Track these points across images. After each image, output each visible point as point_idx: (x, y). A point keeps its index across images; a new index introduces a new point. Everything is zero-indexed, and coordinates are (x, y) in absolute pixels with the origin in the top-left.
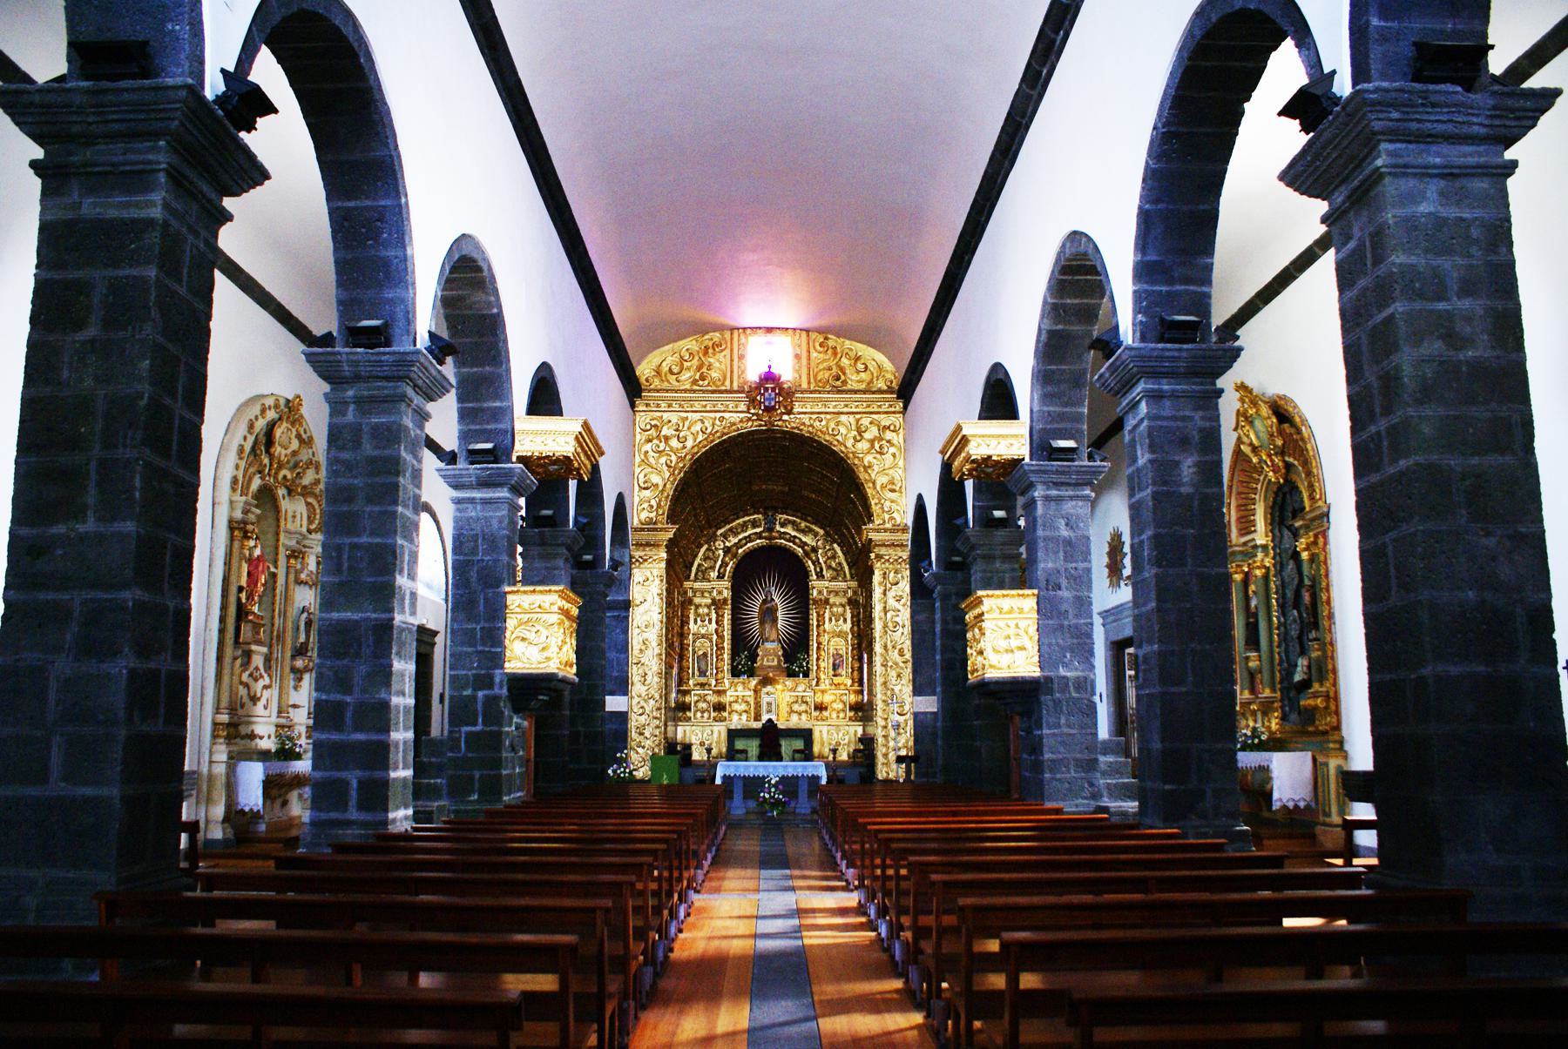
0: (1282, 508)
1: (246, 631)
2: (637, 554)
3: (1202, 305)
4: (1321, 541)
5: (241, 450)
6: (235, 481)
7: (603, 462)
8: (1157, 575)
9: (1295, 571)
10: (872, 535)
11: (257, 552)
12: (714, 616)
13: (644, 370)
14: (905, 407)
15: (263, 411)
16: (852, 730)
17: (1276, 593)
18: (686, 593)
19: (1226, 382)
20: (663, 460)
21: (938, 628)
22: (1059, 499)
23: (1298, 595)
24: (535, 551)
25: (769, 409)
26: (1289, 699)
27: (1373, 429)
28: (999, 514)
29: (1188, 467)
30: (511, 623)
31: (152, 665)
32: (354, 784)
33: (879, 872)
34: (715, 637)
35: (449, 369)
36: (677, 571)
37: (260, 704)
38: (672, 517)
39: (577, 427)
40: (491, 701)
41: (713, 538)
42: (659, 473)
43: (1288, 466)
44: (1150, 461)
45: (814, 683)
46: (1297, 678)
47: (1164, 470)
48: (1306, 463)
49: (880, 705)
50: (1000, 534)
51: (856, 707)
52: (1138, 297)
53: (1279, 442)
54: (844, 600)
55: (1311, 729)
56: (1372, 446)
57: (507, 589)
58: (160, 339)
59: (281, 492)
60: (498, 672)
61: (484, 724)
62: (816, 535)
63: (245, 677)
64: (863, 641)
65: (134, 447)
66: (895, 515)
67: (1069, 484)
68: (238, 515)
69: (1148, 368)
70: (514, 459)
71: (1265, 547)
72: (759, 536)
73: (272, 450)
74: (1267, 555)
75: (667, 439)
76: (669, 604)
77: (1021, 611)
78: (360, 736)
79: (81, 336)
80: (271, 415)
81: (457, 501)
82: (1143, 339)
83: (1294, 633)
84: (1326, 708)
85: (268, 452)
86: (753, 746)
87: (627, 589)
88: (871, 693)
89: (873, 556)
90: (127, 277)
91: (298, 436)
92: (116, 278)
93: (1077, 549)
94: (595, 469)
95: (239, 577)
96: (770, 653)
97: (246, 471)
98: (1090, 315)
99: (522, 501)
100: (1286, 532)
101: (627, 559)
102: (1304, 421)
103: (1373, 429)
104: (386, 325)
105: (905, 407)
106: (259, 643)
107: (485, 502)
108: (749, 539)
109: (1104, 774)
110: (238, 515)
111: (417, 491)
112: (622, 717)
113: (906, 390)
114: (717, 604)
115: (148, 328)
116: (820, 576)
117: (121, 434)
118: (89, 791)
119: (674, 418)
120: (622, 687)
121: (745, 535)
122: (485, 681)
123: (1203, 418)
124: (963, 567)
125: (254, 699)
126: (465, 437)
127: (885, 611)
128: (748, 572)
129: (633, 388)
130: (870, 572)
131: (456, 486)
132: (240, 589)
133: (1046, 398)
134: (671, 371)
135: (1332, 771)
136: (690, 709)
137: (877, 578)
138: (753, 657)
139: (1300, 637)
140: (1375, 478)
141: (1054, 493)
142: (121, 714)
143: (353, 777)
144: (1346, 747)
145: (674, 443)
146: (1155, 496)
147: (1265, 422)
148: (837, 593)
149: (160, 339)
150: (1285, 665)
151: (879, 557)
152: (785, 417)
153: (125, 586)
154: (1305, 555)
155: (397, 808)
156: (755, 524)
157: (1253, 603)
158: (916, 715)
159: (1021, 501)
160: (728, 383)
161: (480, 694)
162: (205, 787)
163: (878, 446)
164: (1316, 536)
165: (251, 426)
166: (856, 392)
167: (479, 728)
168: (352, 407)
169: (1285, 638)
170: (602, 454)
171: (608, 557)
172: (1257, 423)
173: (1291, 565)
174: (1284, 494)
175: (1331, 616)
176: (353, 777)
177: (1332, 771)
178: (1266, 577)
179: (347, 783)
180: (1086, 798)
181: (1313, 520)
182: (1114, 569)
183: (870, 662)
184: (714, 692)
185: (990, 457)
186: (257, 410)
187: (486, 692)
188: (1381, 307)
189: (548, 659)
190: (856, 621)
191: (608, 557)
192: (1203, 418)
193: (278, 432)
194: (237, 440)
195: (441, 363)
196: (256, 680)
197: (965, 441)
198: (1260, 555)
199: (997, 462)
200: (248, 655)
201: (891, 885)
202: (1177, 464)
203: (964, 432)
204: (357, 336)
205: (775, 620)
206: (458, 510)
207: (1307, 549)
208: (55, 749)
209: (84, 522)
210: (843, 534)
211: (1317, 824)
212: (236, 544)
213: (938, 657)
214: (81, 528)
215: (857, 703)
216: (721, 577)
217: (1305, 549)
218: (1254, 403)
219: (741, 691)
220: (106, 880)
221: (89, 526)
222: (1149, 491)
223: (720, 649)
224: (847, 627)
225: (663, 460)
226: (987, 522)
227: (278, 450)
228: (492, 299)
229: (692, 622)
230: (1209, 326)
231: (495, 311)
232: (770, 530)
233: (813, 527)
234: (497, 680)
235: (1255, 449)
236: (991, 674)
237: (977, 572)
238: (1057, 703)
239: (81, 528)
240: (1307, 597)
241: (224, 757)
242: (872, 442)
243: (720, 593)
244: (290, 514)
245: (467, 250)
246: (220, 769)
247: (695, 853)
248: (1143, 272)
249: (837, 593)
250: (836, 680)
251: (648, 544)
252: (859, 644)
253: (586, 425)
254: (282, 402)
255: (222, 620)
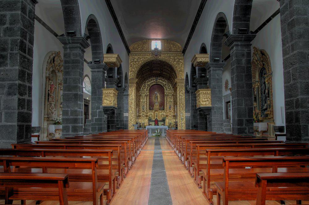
0: (262, 73)
1: (50, 99)
2: (130, 85)
3: (248, 26)
4: (270, 79)
5: (48, 62)
6: (47, 68)
7: (122, 64)
8: (237, 83)
9: (264, 86)
10: (177, 81)
11: (52, 83)
12: (145, 98)
13: (131, 48)
14: (184, 55)
15: (52, 54)
16: (173, 120)
17: (260, 91)
18: (140, 93)
19: (252, 47)
20: (135, 66)
21: (190, 99)
22: (216, 70)
23: (265, 91)
24: (109, 83)
25: (156, 55)
26: (263, 112)
27: (288, 45)
28: (203, 75)
29: (244, 60)
30: (103, 96)
31: (23, 97)
32: (71, 127)
33: (178, 144)
34: (146, 102)
35: (89, 41)
36: (138, 89)
37: (54, 114)
38: (137, 78)
39: (116, 56)
40: (100, 112)
41: (145, 82)
42: (134, 69)
43: (263, 64)
44: (236, 59)
45: (165, 111)
46: (264, 108)
47: (239, 62)
48: (268, 63)
49: (179, 115)
50: (203, 79)
51: (174, 116)
52: (234, 24)
53: (262, 59)
54: (171, 95)
55: (267, 118)
56: (287, 49)
57: (103, 89)
58: (22, 27)
59: (57, 71)
60: (101, 106)
61: (99, 117)
62: (166, 82)
63: (50, 108)
64: (175, 103)
65: (17, 50)
66: (182, 77)
67: (218, 67)
68: (48, 75)
69: (236, 39)
70: (104, 63)
71: (258, 81)
72: (154, 82)
73: (54, 63)
74: (258, 83)
75: (136, 61)
76: (137, 95)
77: (208, 93)
78: (72, 117)
79: (5, 26)
80: (54, 55)
81: (92, 71)
82: (235, 33)
83: (264, 99)
84: (271, 113)
85: (53, 63)
86: (153, 123)
87: (128, 92)
88: (177, 113)
89: (177, 85)
90: (14, 13)
91: (60, 60)
92: (12, 14)
93: (219, 80)
94: (120, 65)
95: (48, 88)
96: (157, 106)
97: (49, 66)
98: (223, 31)
99: (106, 72)
100: (263, 78)
101: (128, 86)
102: (267, 55)
103: (288, 45)
104: (75, 32)
105: (184, 55)
106: (53, 102)
107: (98, 71)
108: (152, 83)
109: (225, 127)
110: (48, 75)
111: (83, 67)
112: (127, 117)
113: (184, 52)
114: (146, 96)
115: (19, 25)
116: (167, 90)
117: (15, 47)
118: (10, 124)
119: (137, 57)
120: (127, 111)
121: (151, 82)
122: (98, 108)
123: (247, 50)
124: (195, 87)
125: (52, 113)
126: (93, 58)
127: (180, 96)
128: (152, 90)
129: (129, 51)
130: (177, 88)
131: (92, 69)
132: (49, 90)
133: (213, 49)
134: (136, 48)
135: (272, 126)
136: (141, 116)
137: (178, 89)
138: (153, 106)
139: (265, 100)
140: (287, 56)
141: (215, 69)
142: (17, 107)
143: (70, 125)
144: (275, 122)
145: (137, 63)
146: (237, 67)
147: (259, 55)
148: (170, 93)
149: (22, 27)
150: (262, 105)
151: (178, 85)
152: (159, 57)
153: (16, 80)
154: (267, 83)
155: (80, 132)
156: (153, 80)
157: (255, 93)
158: (186, 117)
159: (208, 71)
160: (148, 50)
161: (98, 110)
162: (42, 130)
163: (178, 63)
164: (269, 78)
165: (50, 57)
166: (173, 52)
167: (97, 117)
168: (68, 49)
169: (262, 100)
170: (122, 62)
171: (124, 85)
172: (258, 55)
173: (264, 85)
174: (262, 70)
175: (272, 95)
176: (70, 125)
177: (272, 126)
178: (258, 88)
179: (72, 131)
180: (221, 131)
181: (269, 75)
182: (226, 87)
183: (177, 107)
184: (146, 113)
185: (201, 61)
186: (51, 54)
187: (99, 110)
188: (291, 17)
189: (111, 103)
190: (174, 99)
191: (124, 85)
192: (247, 50)
193: (55, 59)
194: (47, 60)
195: (87, 40)
196: (53, 109)
197: (196, 58)
198: (257, 83)
199: (203, 63)
200: (51, 104)
201: (181, 146)
202: (241, 60)
203: (196, 56)
204: (69, 34)
205: (158, 99)
206: (92, 73)
207: (267, 81)
208: (3, 115)
209: (7, 67)
210: (171, 82)
211: (268, 137)
212: (47, 81)
213: (190, 105)
214: (7, 68)
215: (174, 115)
216: (147, 90)
217: (267, 81)
218: (257, 51)
219: (151, 113)
220: (15, 142)
221: (8, 67)
222: (235, 65)
223: (147, 104)
224: (172, 100)
225: (135, 66)
226: (202, 77)
227: (55, 62)
228: (98, 29)
229: (141, 99)
230: (249, 30)
231: (99, 32)
232: (156, 81)
233: (165, 80)
234: (101, 108)
235: (256, 61)
236: (201, 106)
237: (198, 87)
238: (215, 112)
239: (7, 68)
240: (267, 91)
241: (46, 124)
242: (177, 62)
243: (147, 93)
244: (59, 76)
245: (92, 18)
246: (46, 126)
247: (141, 142)
248: (235, 19)
249: (170, 93)
250: (170, 111)
251: (132, 83)
252: (175, 103)
253: (118, 55)
254: (56, 53)
255: (45, 96)
